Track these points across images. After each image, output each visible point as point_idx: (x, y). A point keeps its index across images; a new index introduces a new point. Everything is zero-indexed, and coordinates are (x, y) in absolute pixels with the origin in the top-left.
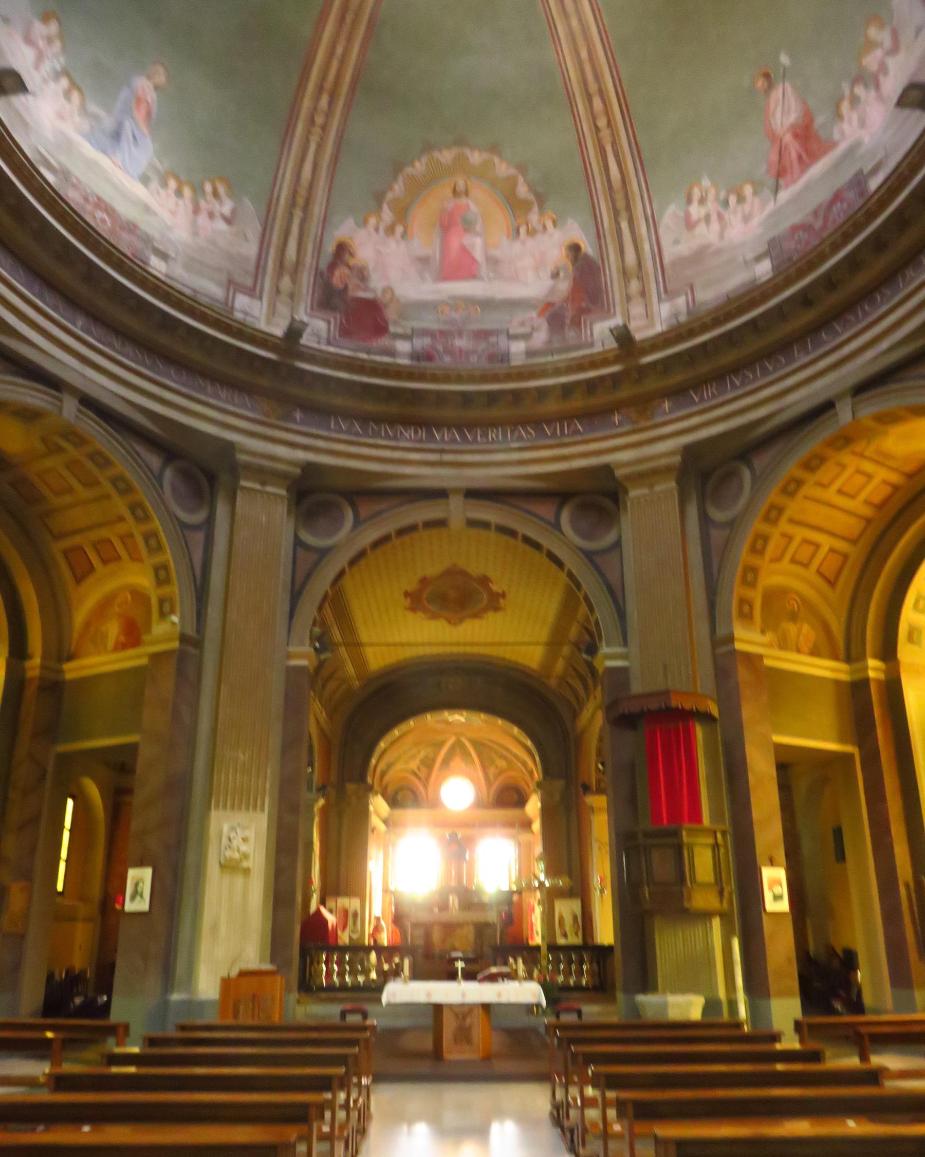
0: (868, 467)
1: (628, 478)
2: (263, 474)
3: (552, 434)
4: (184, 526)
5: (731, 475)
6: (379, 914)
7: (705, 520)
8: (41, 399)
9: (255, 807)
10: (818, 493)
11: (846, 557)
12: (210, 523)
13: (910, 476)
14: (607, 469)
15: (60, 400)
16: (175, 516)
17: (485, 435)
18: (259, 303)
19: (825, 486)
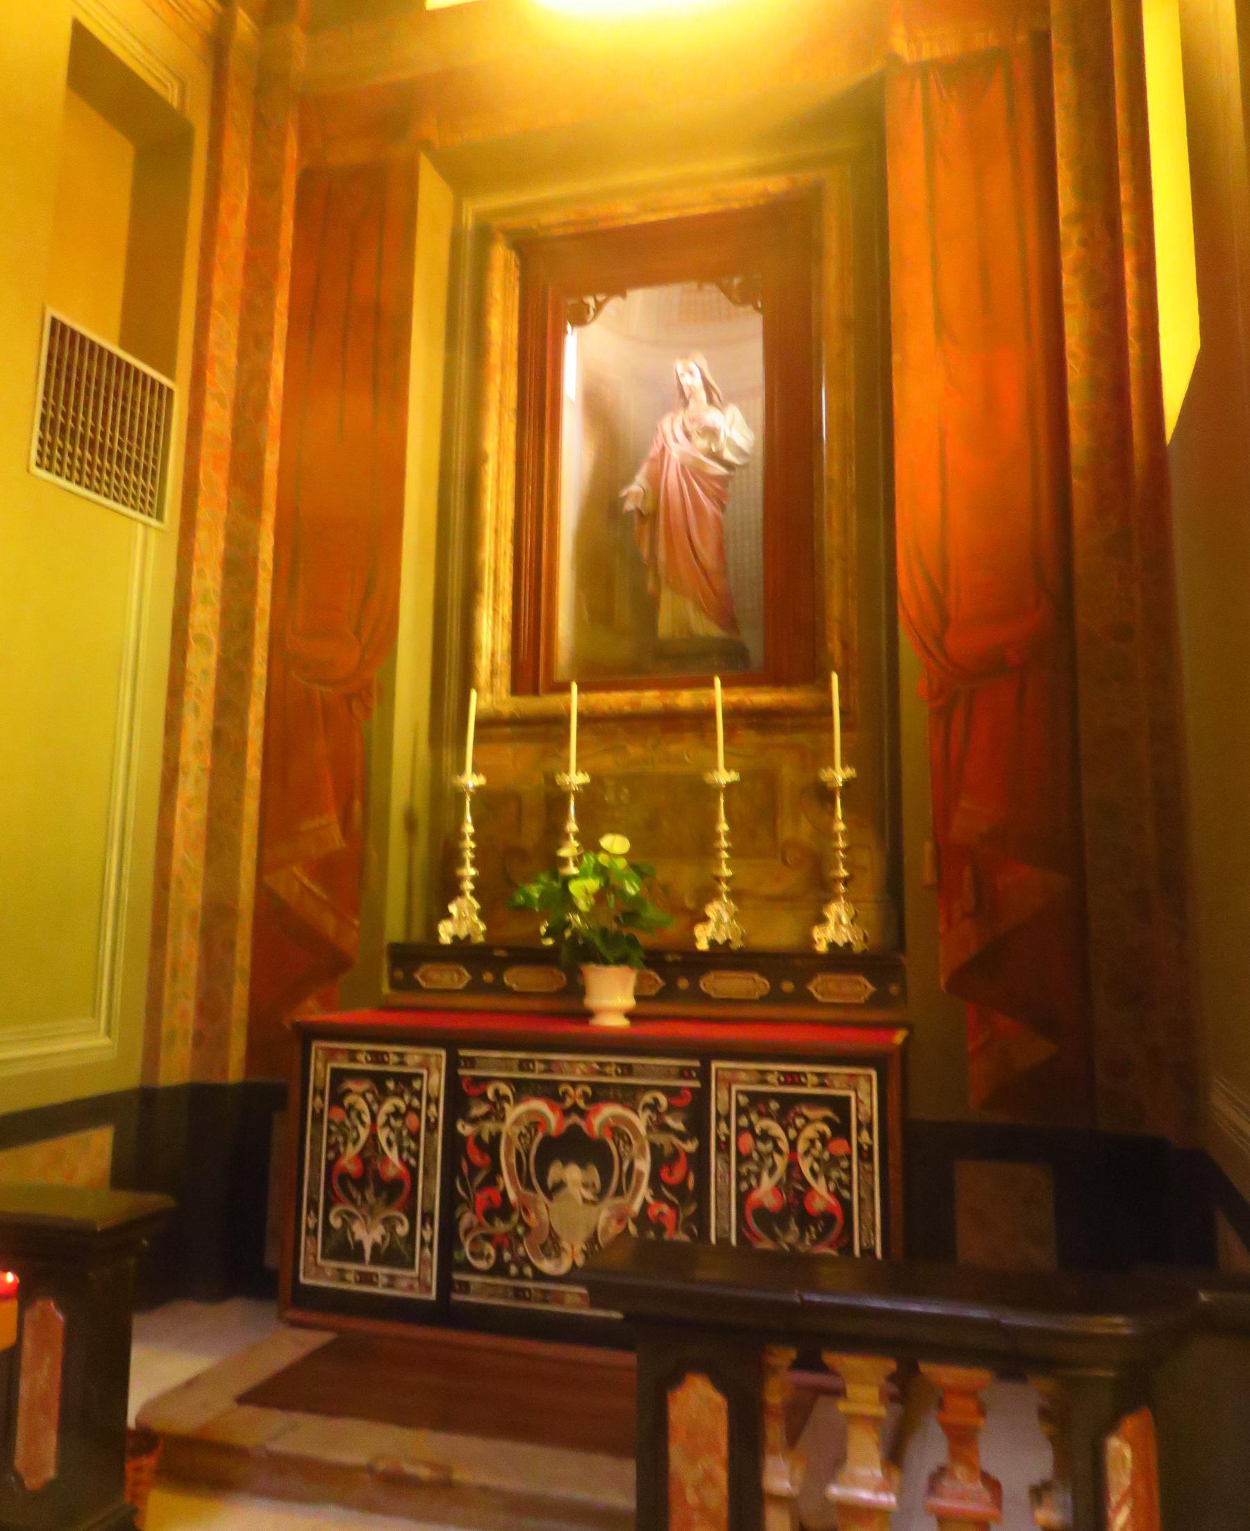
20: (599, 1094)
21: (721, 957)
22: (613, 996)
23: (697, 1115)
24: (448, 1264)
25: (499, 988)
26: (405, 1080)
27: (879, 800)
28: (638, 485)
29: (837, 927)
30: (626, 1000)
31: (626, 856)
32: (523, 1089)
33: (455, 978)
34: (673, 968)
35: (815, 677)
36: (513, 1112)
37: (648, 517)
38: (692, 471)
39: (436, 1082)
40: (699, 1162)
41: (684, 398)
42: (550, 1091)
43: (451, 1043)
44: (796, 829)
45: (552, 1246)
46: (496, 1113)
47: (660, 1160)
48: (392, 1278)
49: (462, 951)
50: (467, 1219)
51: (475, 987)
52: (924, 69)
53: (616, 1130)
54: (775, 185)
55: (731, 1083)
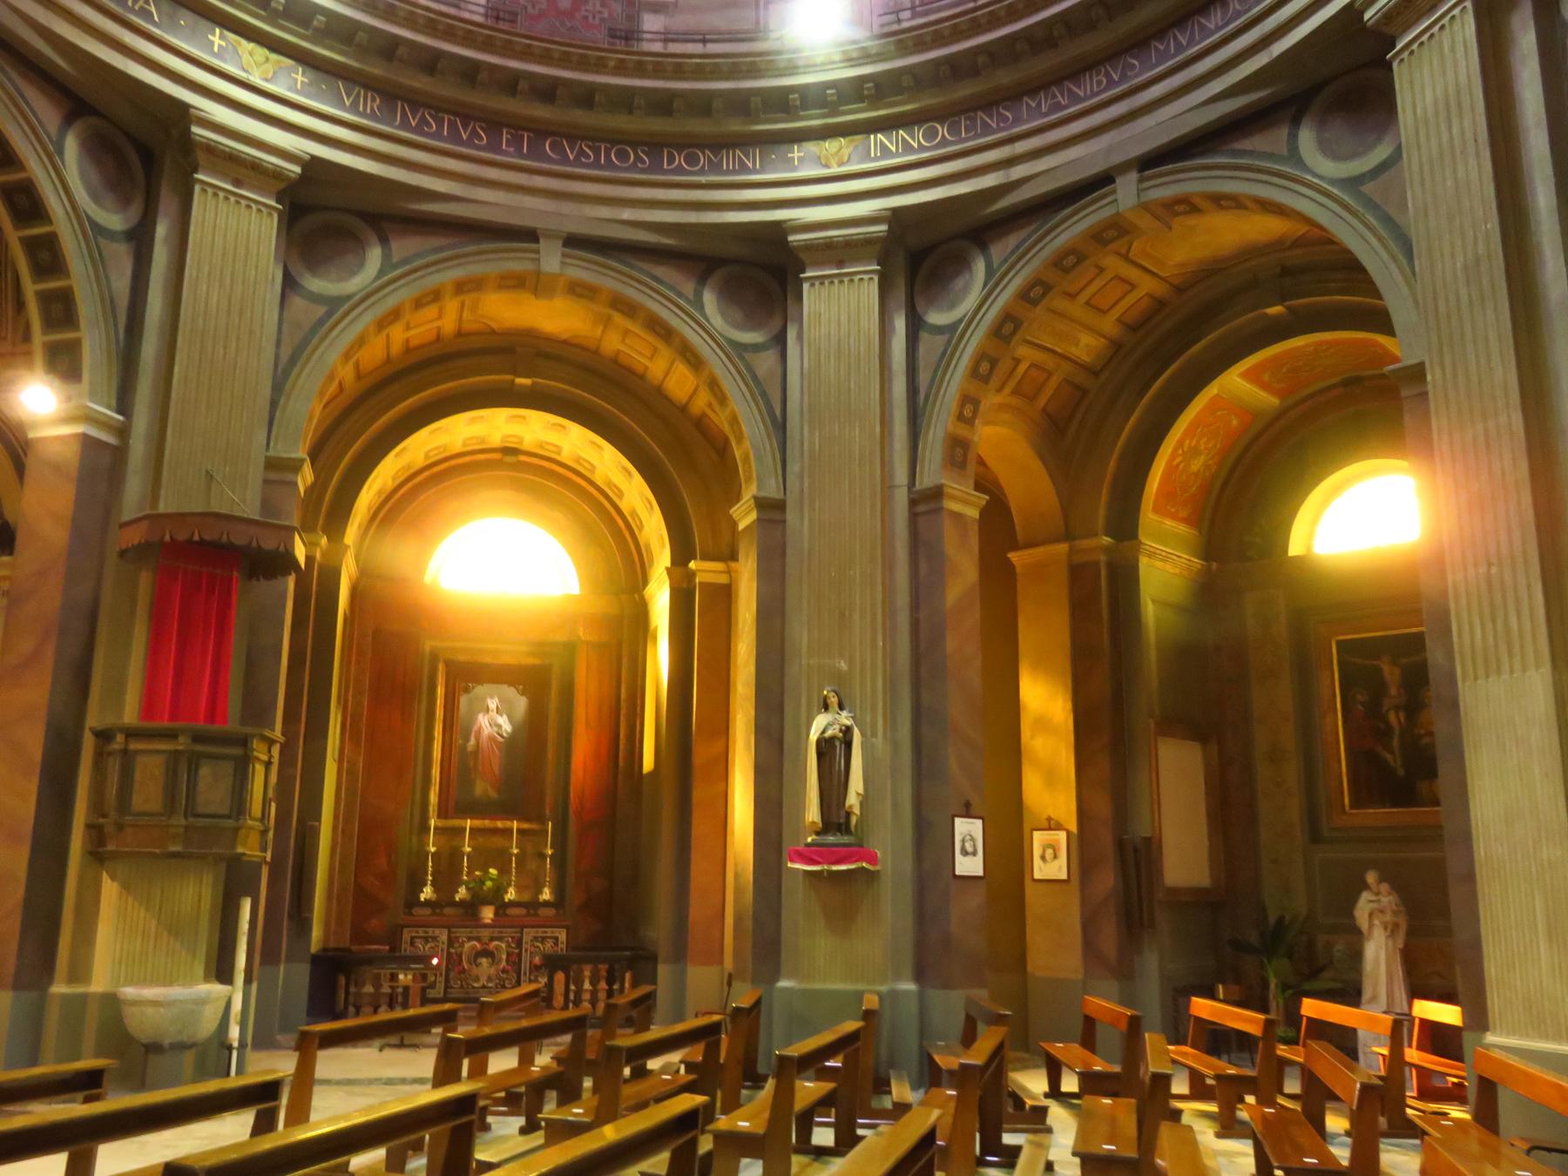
0: (1132, 273)
1: (810, 247)
2: (242, 170)
3: (469, 138)
4: (99, 230)
5: (961, 263)
6: (424, 1062)
7: (915, 325)
8: (1498, 543)
9: (1499, 671)
10: (1060, 303)
11: (1084, 392)
12: (140, 238)
13: (1180, 290)
14: (778, 231)
15: (538, 252)
16: (88, 217)
17: (671, 160)
18: (140, 759)
19: (1072, 296)
20: (492, 939)
21: (512, 904)
22: (488, 914)
23: (519, 943)
24: (446, 987)
25: (441, 914)
26: (434, 938)
27: (560, 861)
28: (472, 741)
29: (546, 895)
30: (491, 915)
31: (1348, 1134)
32: (470, 939)
33: (427, 911)
34: (502, 907)
35: (541, 820)
36: (467, 945)
37: (476, 752)
38: (491, 738)
39: (444, 938)
40: (520, 955)
41: (488, 710)
42: (478, 939)
43: (448, 927)
44: (532, 865)
45: (477, 979)
46: (462, 945)
47: (509, 955)
48: (965, 853)
49: (428, 903)
50: (452, 975)
51: (433, 914)
52: (588, 643)
53: (497, 948)
54: (537, 661)
55: (528, 934)
